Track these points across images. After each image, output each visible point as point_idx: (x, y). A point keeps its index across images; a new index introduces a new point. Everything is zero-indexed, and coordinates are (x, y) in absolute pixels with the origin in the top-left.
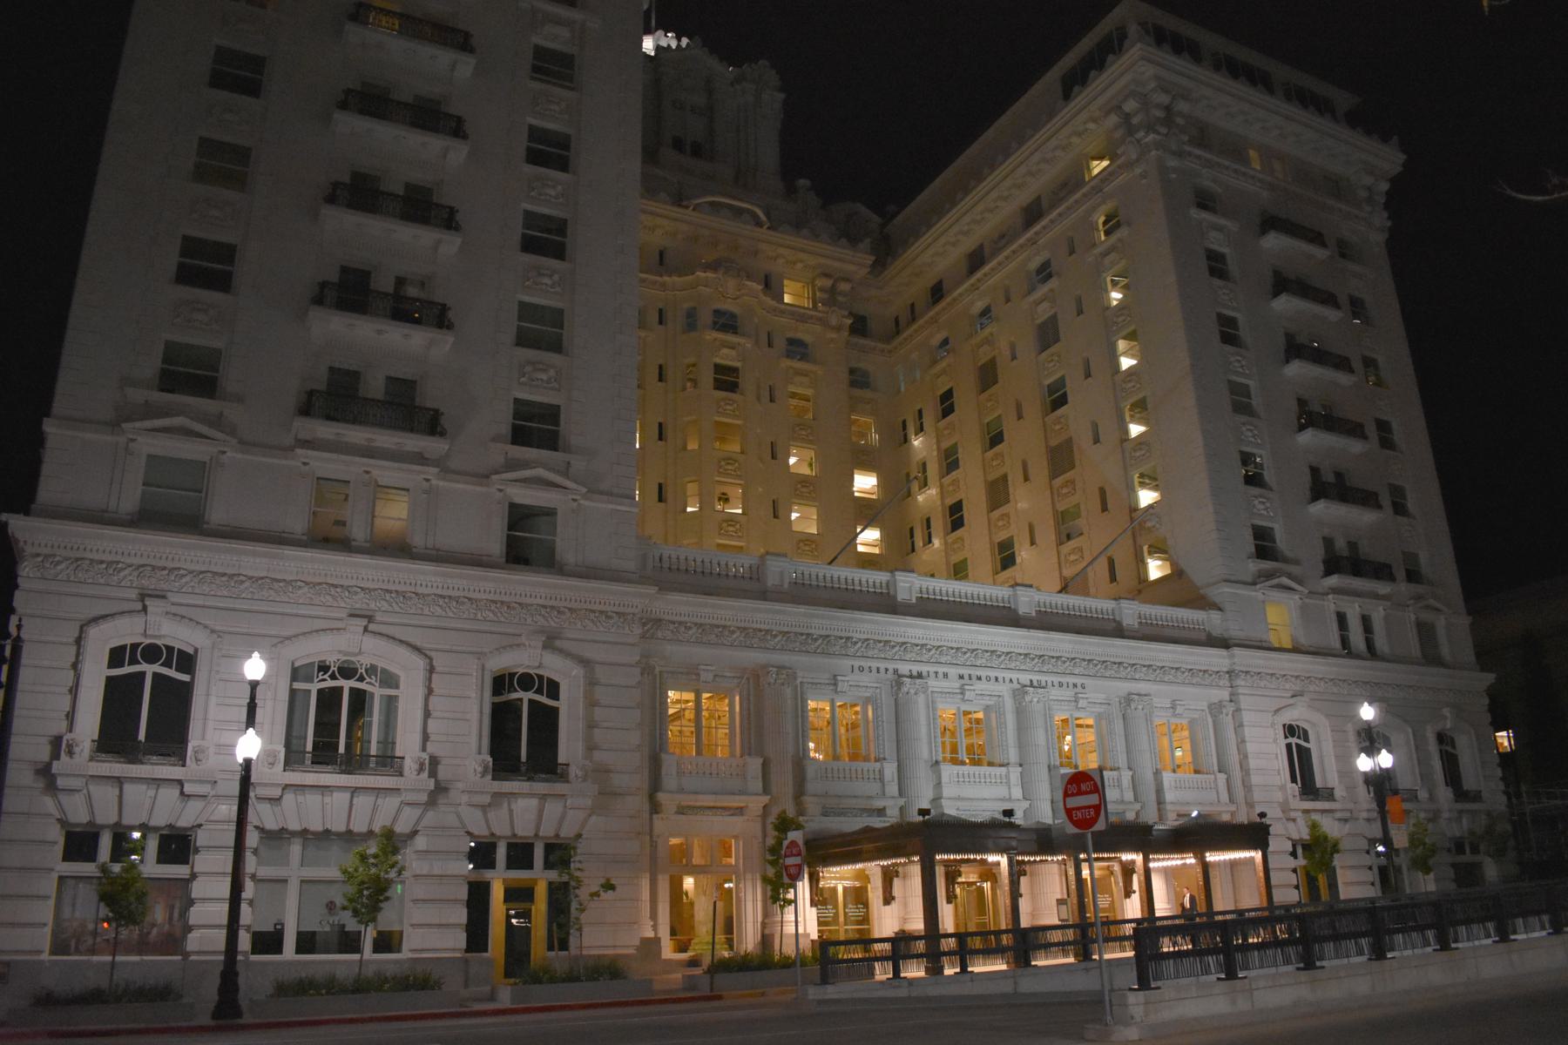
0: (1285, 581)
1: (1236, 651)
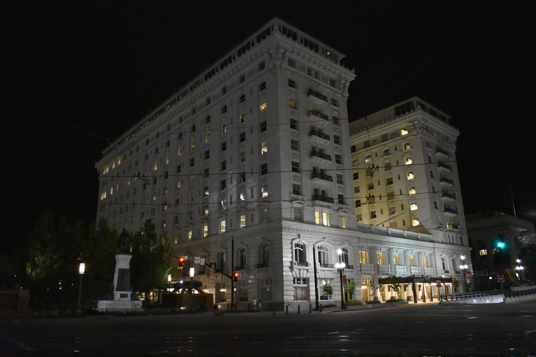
0: (442, 229)
1: (436, 244)
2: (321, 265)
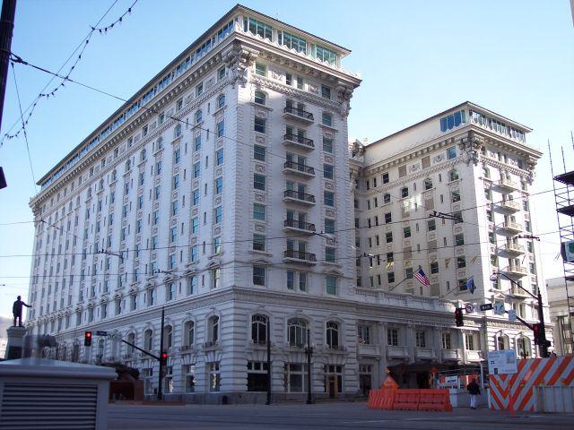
2: (255, 342)
